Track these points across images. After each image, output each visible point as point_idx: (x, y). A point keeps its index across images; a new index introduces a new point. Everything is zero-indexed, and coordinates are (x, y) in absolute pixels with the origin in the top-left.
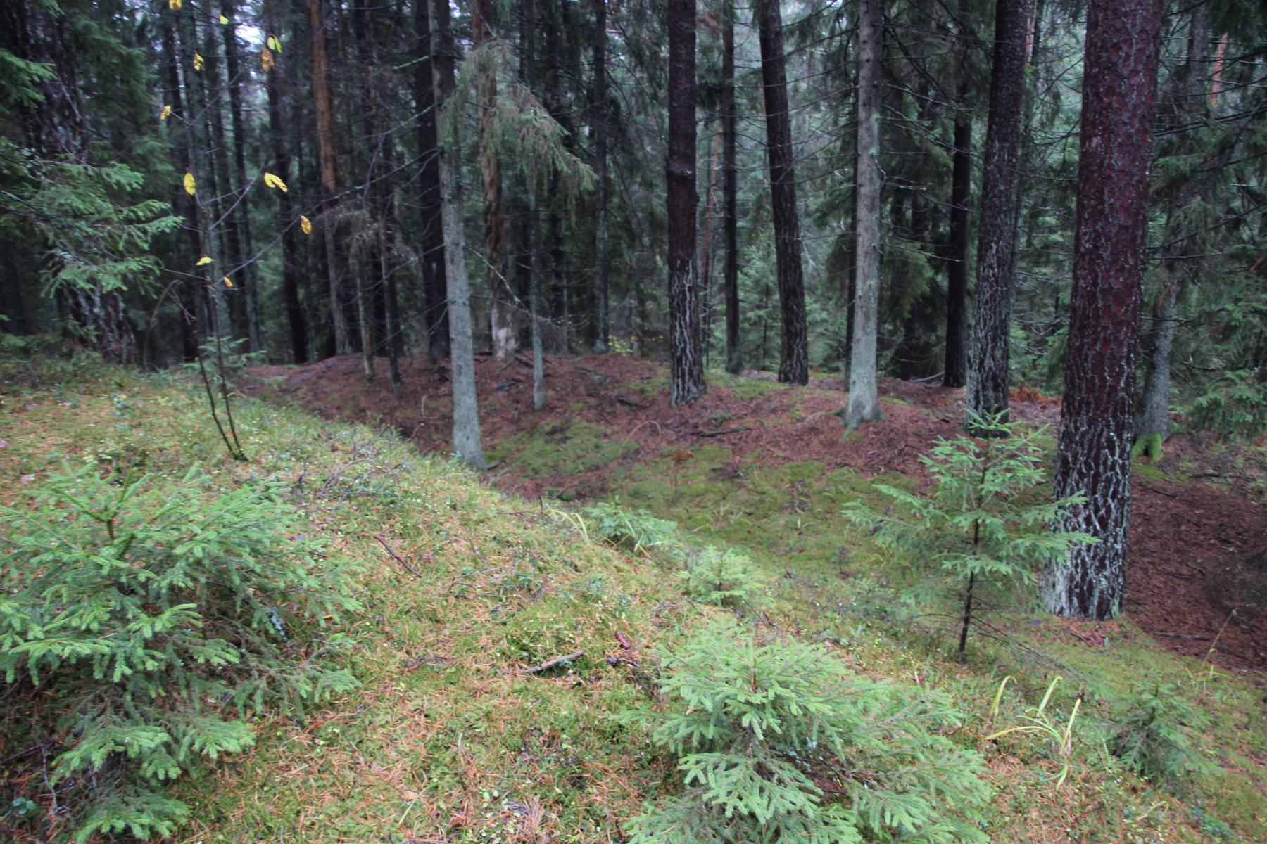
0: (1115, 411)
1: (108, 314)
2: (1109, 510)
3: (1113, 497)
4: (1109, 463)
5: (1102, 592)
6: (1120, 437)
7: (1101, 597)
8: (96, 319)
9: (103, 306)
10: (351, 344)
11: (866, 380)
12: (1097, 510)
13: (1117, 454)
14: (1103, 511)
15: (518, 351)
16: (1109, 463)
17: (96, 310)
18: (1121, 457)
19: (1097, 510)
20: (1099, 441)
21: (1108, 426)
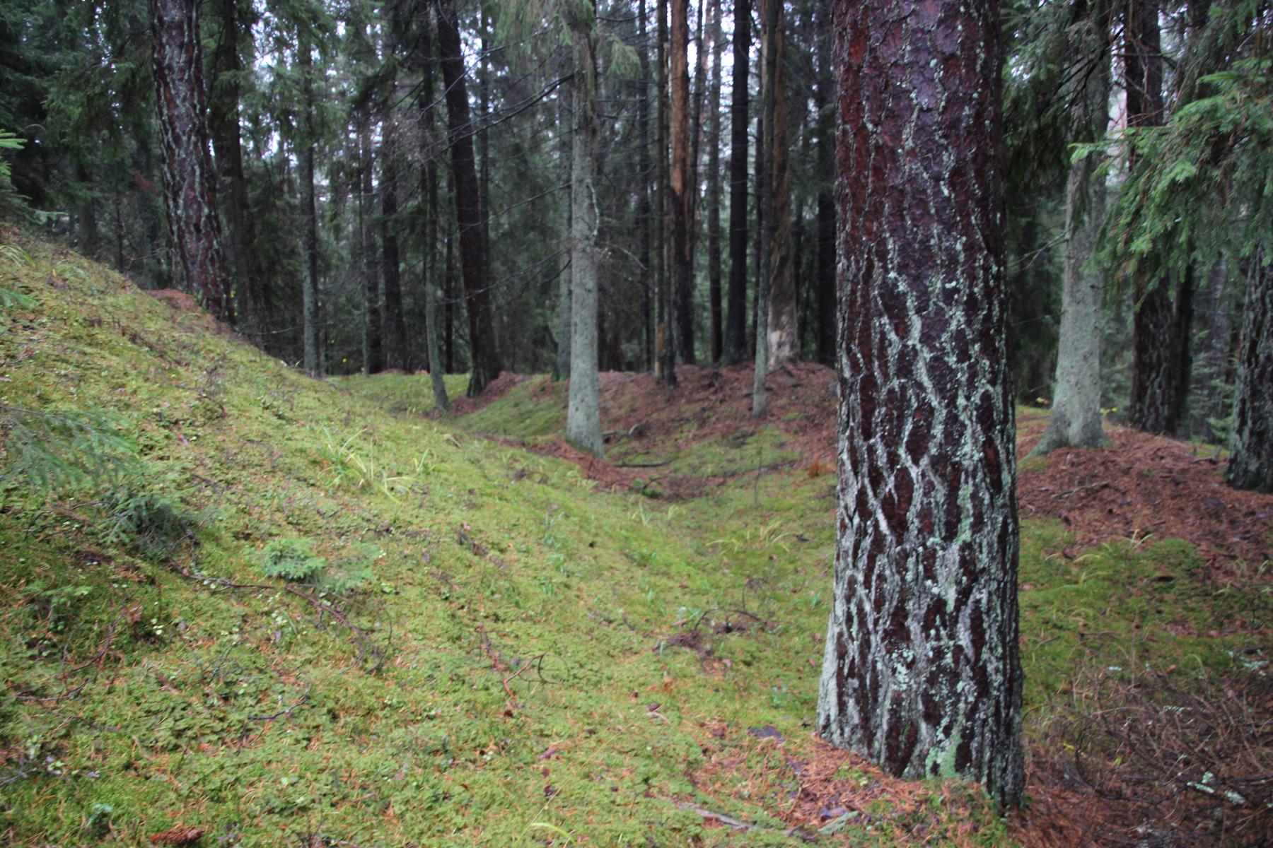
0: (899, 213)
1: (188, 217)
2: (904, 483)
3: (916, 450)
4: (892, 352)
5: (897, 700)
6: (917, 281)
7: (893, 712)
8: (179, 219)
9: (186, 208)
10: (682, 354)
11: (1073, 379)
12: (876, 479)
13: (916, 332)
14: (890, 484)
15: (792, 360)
16: (892, 352)
17: (179, 212)
18: (926, 339)
19: (876, 479)
20: (865, 296)
21: (883, 256)
